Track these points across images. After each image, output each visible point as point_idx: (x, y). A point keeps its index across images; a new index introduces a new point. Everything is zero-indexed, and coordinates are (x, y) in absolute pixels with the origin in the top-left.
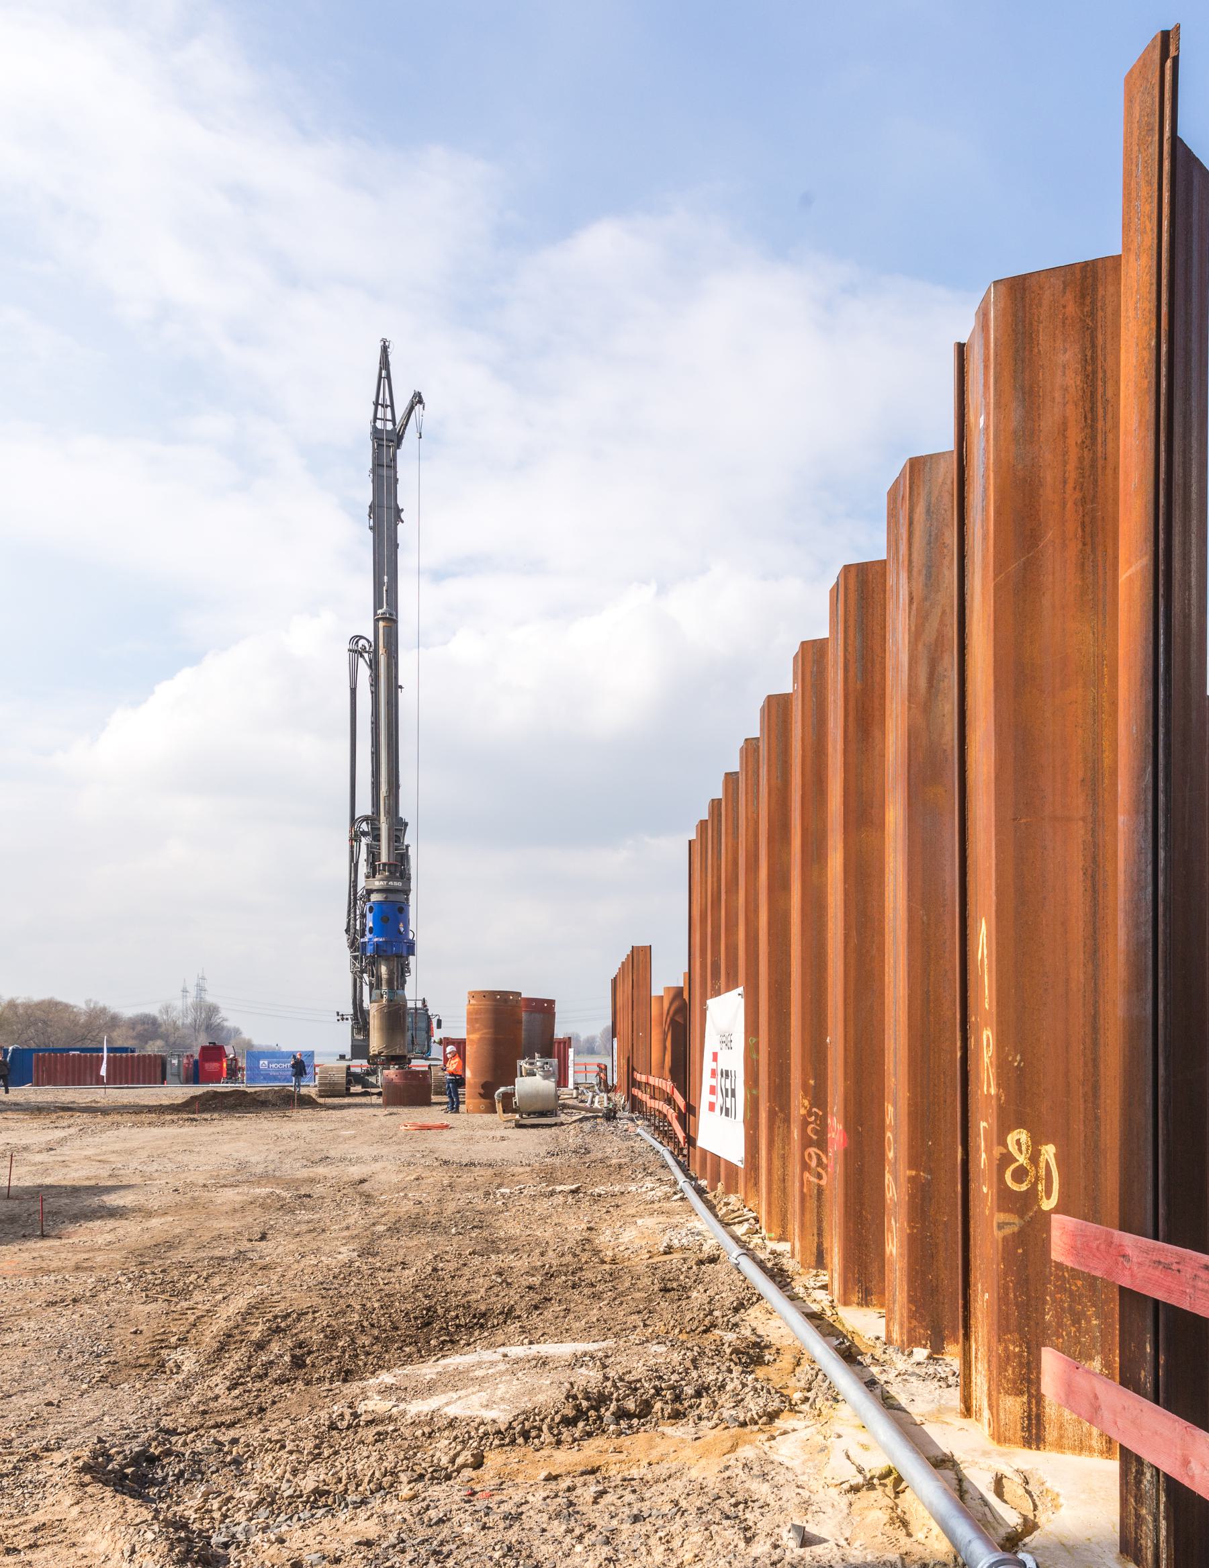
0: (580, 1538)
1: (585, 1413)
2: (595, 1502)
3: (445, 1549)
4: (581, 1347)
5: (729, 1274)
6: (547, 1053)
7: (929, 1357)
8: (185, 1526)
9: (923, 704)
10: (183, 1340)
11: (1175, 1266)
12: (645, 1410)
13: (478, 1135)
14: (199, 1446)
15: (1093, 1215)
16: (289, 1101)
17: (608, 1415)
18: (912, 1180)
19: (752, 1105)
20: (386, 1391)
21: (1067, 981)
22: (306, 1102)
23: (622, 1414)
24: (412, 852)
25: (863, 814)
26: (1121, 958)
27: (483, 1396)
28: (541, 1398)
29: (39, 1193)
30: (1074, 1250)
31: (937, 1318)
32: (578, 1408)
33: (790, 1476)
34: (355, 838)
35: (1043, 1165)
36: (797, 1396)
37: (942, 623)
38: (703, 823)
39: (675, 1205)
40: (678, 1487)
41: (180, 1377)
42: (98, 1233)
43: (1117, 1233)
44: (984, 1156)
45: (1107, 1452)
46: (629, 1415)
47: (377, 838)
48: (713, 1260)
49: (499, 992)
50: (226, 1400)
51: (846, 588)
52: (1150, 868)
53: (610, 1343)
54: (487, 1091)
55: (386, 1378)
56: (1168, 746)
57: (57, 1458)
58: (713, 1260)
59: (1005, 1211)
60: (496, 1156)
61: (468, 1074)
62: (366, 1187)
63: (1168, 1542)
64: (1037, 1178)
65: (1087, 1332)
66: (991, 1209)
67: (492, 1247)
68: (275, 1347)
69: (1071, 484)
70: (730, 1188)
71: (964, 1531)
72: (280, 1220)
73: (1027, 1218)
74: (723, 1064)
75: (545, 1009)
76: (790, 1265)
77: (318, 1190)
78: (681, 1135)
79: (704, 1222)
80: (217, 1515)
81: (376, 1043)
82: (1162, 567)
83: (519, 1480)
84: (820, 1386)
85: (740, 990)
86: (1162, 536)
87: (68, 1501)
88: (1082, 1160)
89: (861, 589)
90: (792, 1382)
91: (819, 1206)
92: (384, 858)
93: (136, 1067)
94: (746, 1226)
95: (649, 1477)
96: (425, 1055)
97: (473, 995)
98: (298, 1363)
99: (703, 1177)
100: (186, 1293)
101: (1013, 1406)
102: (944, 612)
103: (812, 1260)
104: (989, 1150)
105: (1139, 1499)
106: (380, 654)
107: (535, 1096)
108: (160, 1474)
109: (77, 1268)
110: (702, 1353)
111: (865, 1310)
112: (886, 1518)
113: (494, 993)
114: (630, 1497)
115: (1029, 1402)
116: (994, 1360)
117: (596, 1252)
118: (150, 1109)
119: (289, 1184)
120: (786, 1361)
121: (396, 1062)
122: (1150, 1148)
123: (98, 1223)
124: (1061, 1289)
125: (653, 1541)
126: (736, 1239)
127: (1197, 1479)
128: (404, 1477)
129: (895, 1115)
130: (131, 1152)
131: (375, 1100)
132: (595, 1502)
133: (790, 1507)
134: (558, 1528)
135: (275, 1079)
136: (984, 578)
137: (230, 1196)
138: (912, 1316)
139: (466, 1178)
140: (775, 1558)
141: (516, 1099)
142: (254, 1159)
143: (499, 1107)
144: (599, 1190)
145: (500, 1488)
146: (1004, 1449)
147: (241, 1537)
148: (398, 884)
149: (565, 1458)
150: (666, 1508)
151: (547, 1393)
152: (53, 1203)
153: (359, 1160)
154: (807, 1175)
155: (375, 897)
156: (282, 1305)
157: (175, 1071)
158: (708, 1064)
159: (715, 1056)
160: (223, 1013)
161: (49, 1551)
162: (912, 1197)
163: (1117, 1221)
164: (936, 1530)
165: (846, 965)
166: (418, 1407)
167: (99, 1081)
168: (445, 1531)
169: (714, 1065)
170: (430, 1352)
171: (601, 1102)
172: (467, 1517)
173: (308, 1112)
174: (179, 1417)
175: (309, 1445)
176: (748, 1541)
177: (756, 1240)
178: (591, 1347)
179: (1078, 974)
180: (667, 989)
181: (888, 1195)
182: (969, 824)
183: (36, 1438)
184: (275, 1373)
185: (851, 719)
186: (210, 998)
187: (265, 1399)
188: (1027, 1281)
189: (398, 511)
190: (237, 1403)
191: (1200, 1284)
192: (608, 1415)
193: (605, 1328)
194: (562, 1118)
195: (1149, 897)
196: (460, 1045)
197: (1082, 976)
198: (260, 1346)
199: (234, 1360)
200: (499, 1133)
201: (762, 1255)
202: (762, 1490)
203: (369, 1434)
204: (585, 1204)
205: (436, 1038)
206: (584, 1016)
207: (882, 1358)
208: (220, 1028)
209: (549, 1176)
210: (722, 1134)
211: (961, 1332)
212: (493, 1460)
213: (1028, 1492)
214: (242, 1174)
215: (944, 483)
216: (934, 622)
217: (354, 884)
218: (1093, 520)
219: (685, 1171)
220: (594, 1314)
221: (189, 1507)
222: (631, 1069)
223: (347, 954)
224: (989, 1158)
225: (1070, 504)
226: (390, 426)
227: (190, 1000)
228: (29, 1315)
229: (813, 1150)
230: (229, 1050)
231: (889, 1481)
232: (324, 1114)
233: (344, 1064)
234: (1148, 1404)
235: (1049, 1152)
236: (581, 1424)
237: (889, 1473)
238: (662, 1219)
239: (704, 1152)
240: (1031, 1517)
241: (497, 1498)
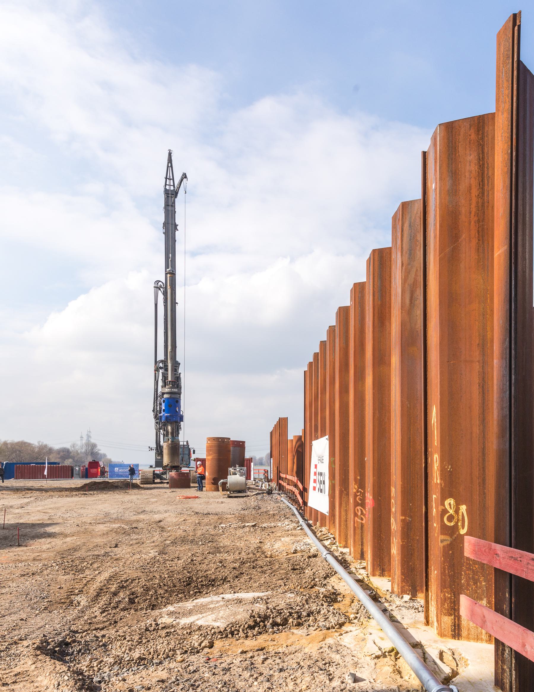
0: (256, 679)
1: (258, 624)
2: (263, 663)
3: (197, 684)
4: (257, 594)
5: (322, 562)
6: (242, 465)
7: (411, 599)
8: (82, 674)
9: (408, 311)
10: (81, 591)
11: (519, 559)
12: (285, 622)
13: (211, 501)
14: (88, 638)
15: (483, 536)
16: (127, 486)
17: (268, 625)
18: (403, 521)
19: (332, 488)
20: (170, 614)
21: (471, 433)
22: (135, 486)
23: (275, 624)
24: (182, 376)
25: (381, 359)
26: (495, 423)
27: (214, 616)
28: (239, 617)
29: (17, 526)
30: (474, 552)
31: (414, 582)
32: (255, 621)
33: (349, 651)
34: (157, 370)
35: (460, 514)
36: (352, 616)
37: (416, 275)
38: (311, 363)
39: (298, 532)
40: (299, 656)
41: (80, 608)
42: (43, 544)
43: (493, 544)
44: (434, 510)
45: (489, 641)
46: (278, 625)
47: (166, 370)
48: (315, 556)
49: (221, 438)
50: (100, 618)
51: (374, 260)
52: (508, 383)
53: (269, 593)
54: (215, 482)
55: (171, 608)
56: (516, 329)
57: (25, 643)
58: (315, 556)
59: (444, 534)
60: (219, 510)
61: (207, 474)
62: (161, 524)
63: (516, 681)
64: (458, 520)
65: (480, 588)
66: (438, 534)
67: (217, 550)
68: (121, 595)
69: (473, 214)
70: (323, 525)
71: (426, 675)
72: (124, 538)
73: (454, 538)
74: (319, 470)
75: (241, 445)
76: (349, 558)
77: (141, 525)
78: (301, 501)
79: (311, 539)
80: (96, 669)
81: (166, 460)
82: (513, 250)
83: (229, 653)
84: (362, 612)
85: (327, 437)
86: (513, 236)
87: (30, 662)
88: (478, 512)
89: (380, 260)
90: (350, 610)
91: (362, 532)
92: (170, 379)
93: (60, 471)
94: (329, 541)
95: (287, 652)
96: (188, 465)
97: (209, 439)
98: (132, 601)
99: (311, 519)
100: (82, 571)
101: (448, 620)
102: (417, 270)
103: (359, 556)
104: (437, 508)
105: (503, 662)
106: (168, 288)
107: (236, 484)
108: (71, 651)
109: (34, 560)
110: (310, 597)
111: (382, 578)
112: (391, 670)
113: (218, 438)
114: (278, 661)
115: (455, 619)
116: (439, 600)
117: (263, 553)
118: (66, 490)
119: (128, 522)
120: (347, 601)
121: (175, 469)
122: (508, 507)
123: (43, 540)
124: (469, 569)
125: (288, 680)
126: (325, 547)
127: (529, 653)
128: (178, 652)
129: (395, 492)
130: (58, 508)
131: (166, 485)
132: (263, 663)
133: (349, 665)
134: (246, 674)
135: (121, 476)
136: (435, 255)
137: (102, 528)
138: (403, 581)
139: (206, 520)
140: (342, 687)
141: (228, 485)
142: (112, 512)
143: (220, 489)
144: (265, 525)
145: (221, 657)
146: (444, 639)
147: (106, 678)
148: (176, 390)
149: (250, 644)
150: (294, 666)
151: (242, 615)
152: (23, 531)
153: (159, 512)
154: (356, 518)
155: (166, 396)
156: (125, 576)
157: (77, 473)
158: (313, 470)
159: (316, 466)
160: (99, 447)
161: (21, 685)
162: (403, 528)
163: (493, 539)
164: (414, 675)
165: (374, 426)
166: (184, 621)
167: (44, 477)
168: (197, 676)
169: (315, 470)
170: (190, 597)
171: (265, 486)
172: (206, 669)
173: (136, 491)
174: (79, 625)
175: (136, 638)
176: (330, 680)
177: (334, 547)
178: (261, 594)
179: (476, 430)
180: (295, 437)
181: (392, 527)
182: (428, 363)
183: (16, 635)
184: (122, 606)
185: (376, 317)
186: (93, 441)
187: (117, 617)
188: (454, 565)
189: (176, 226)
190: (105, 619)
191: (530, 567)
192: (268, 625)
193: (267, 586)
194: (248, 493)
195: (508, 396)
196: (203, 461)
197: (478, 431)
198: (115, 594)
199: (103, 600)
200: (220, 500)
201: (337, 554)
202: (336, 658)
203: (163, 633)
204: (258, 531)
205: (192, 458)
206: (258, 449)
207: (390, 599)
208: (97, 454)
209: (242, 519)
210: (319, 501)
211: (424, 588)
212: (218, 644)
213: (454, 659)
214: (107, 518)
215: (417, 213)
216: (413, 275)
217: (156, 390)
218: (483, 229)
219: (303, 517)
220: (262, 580)
221: (83, 665)
222: (279, 472)
223: (153, 421)
224: (437, 511)
225: (472, 223)
226: (172, 188)
227: (84, 441)
228: (13, 580)
229: (359, 508)
230: (101, 464)
231: (393, 654)
232: (143, 491)
233: (152, 469)
234: (507, 620)
235: (463, 508)
236: (257, 629)
237: (393, 650)
238: (292, 538)
239: (311, 508)
240: (455, 669)
241: (220, 661)
